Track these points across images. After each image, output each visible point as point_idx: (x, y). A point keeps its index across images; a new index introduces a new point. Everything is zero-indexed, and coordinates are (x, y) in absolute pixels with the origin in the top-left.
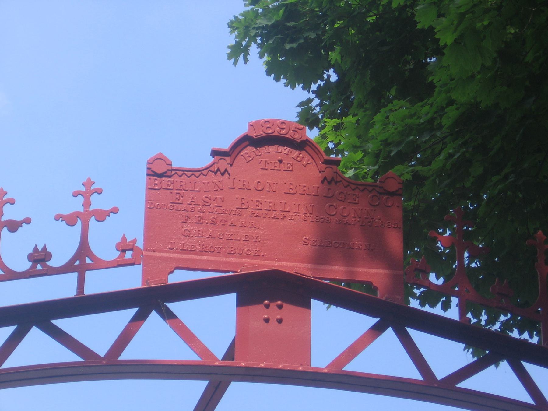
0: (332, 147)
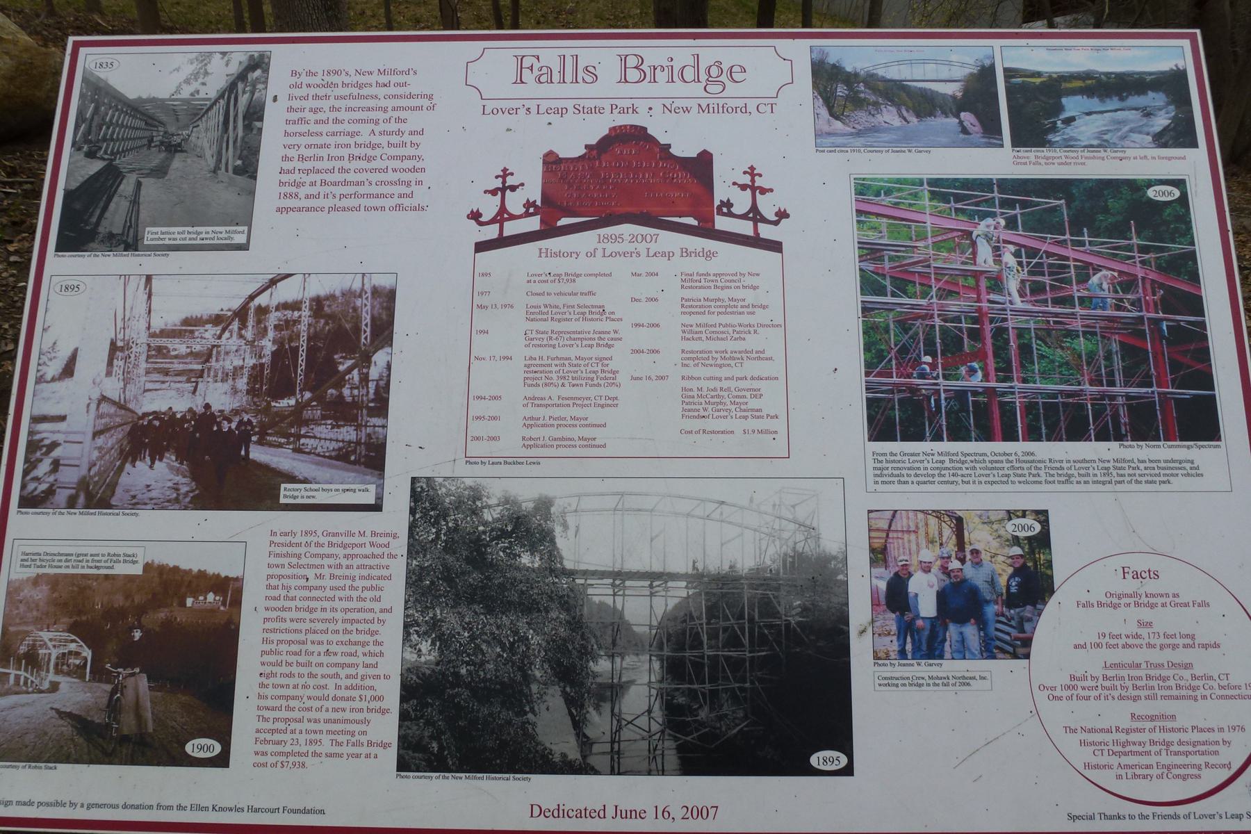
0: (635, 629)
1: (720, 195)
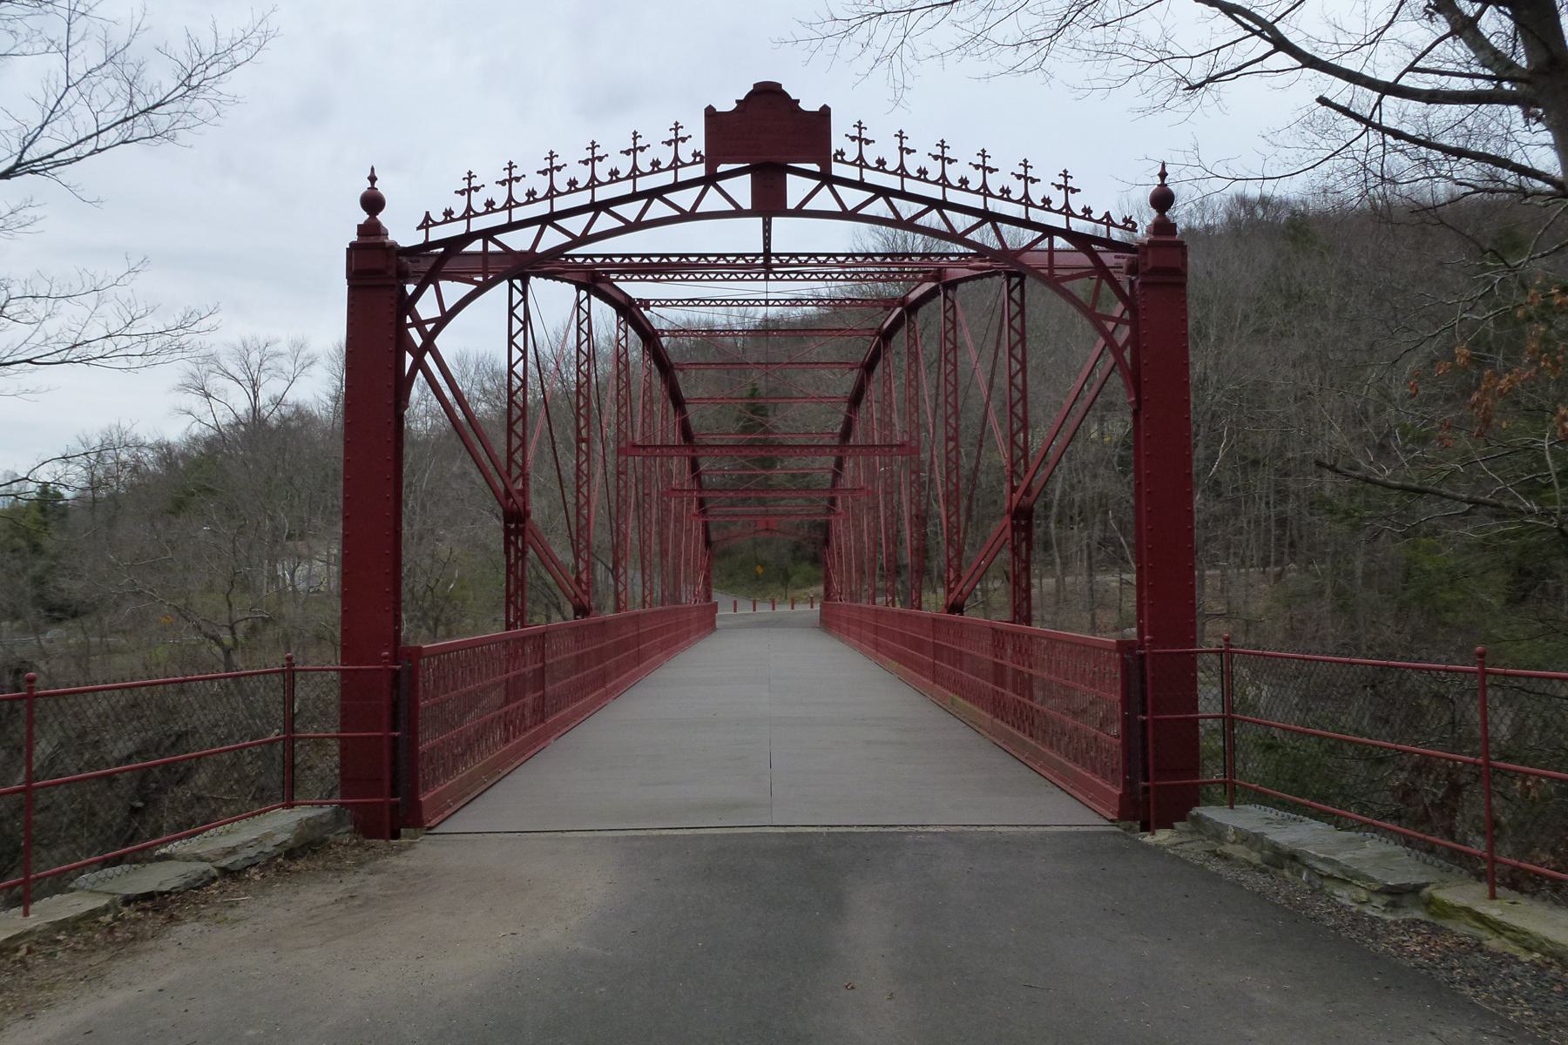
1: (835, 146)
